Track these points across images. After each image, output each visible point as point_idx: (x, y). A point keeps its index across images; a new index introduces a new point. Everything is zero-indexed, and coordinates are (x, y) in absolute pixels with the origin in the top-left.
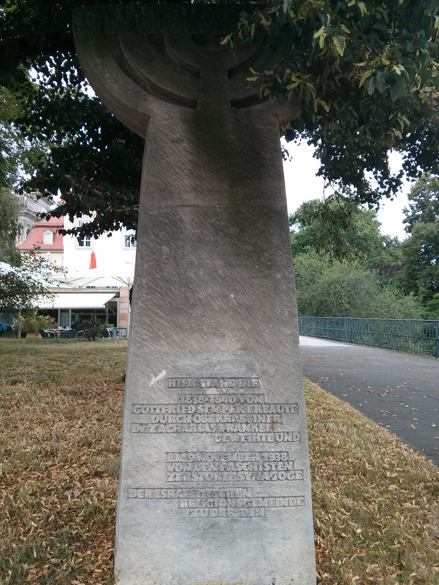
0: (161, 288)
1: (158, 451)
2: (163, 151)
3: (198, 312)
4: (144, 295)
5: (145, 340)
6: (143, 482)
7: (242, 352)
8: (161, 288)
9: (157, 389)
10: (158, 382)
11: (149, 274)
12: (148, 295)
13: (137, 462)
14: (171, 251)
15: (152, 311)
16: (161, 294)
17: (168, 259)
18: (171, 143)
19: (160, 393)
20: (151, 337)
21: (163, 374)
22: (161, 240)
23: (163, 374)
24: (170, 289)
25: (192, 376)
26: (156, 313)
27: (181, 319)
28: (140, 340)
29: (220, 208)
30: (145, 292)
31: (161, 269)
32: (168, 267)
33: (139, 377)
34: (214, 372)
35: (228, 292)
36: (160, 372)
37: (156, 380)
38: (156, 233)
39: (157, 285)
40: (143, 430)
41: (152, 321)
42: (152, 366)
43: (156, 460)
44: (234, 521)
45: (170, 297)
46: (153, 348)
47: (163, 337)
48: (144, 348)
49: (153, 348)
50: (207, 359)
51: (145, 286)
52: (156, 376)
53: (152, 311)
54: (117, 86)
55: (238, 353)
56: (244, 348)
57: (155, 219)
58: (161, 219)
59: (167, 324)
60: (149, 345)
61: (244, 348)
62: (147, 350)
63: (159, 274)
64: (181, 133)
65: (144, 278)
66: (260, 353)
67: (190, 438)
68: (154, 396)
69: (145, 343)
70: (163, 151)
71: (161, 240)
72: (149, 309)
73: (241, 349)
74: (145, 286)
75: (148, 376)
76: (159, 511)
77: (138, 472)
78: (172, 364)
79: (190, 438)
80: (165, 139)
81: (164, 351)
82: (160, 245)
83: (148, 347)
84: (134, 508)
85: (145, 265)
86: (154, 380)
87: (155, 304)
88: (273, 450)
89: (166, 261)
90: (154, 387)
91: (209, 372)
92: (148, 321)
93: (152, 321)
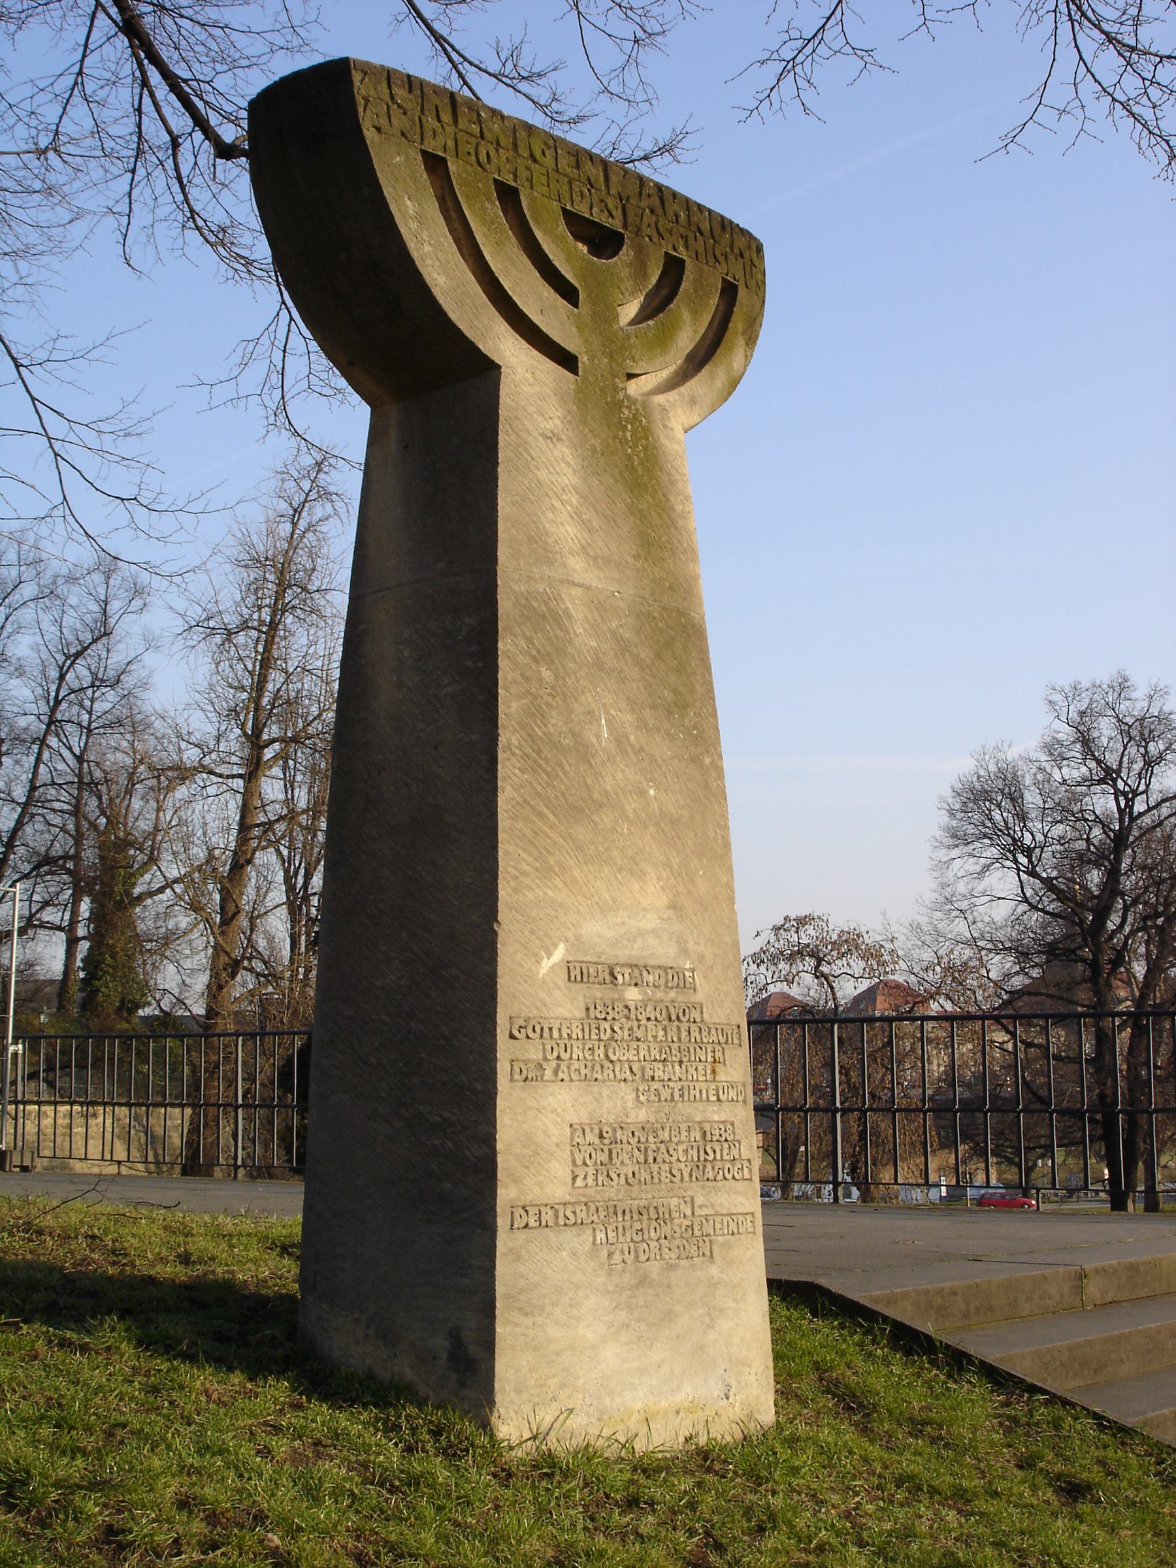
0: (546, 760)
1: (559, 1120)
2: (529, 454)
3: (606, 820)
4: (517, 771)
5: (524, 874)
6: (536, 1189)
7: (671, 913)
8: (546, 760)
9: (552, 985)
10: (552, 968)
11: (520, 724)
12: (523, 773)
13: (525, 1147)
14: (557, 679)
15: (532, 807)
16: (548, 774)
17: (554, 697)
18: (541, 439)
19: (557, 994)
20: (537, 869)
21: (559, 953)
22: (538, 651)
23: (559, 953)
24: (560, 765)
25: (603, 959)
26: (540, 815)
27: (582, 833)
28: (515, 872)
29: (622, 599)
30: (518, 765)
31: (543, 716)
32: (554, 713)
33: (519, 956)
34: (634, 953)
35: (645, 784)
36: (555, 946)
37: (550, 964)
38: (528, 634)
39: (539, 752)
40: (530, 1078)
41: (536, 833)
42: (541, 933)
43: (555, 1140)
44: (671, 1267)
45: (563, 783)
46: (541, 894)
47: (556, 869)
48: (525, 891)
49: (541, 894)
50: (623, 923)
51: (518, 752)
52: (549, 955)
53: (532, 807)
54: (444, 279)
55: (665, 916)
56: (673, 906)
57: (523, 602)
58: (535, 605)
59: (562, 840)
60: (534, 886)
61: (673, 906)
62: (530, 895)
63: (539, 727)
64: (557, 422)
65: (513, 734)
66: (694, 918)
67: (605, 1092)
68: (548, 1000)
69: (527, 881)
70: (529, 454)
71: (538, 651)
72: (528, 803)
73: (669, 907)
74: (518, 752)
75: (536, 955)
76: (565, 1254)
77: (527, 1168)
78: (573, 931)
79: (605, 1092)
80: (531, 428)
81: (560, 900)
82: (537, 662)
83: (530, 888)
84: (523, 1252)
85: (513, 704)
86: (546, 965)
87: (540, 795)
88: (716, 1118)
89: (550, 699)
90: (548, 979)
91: (627, 952)
92: (528, 833)
93: (536, 833)
